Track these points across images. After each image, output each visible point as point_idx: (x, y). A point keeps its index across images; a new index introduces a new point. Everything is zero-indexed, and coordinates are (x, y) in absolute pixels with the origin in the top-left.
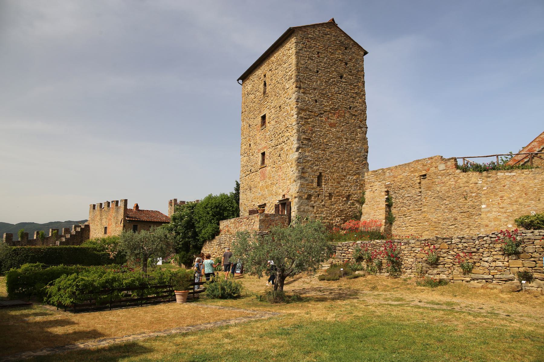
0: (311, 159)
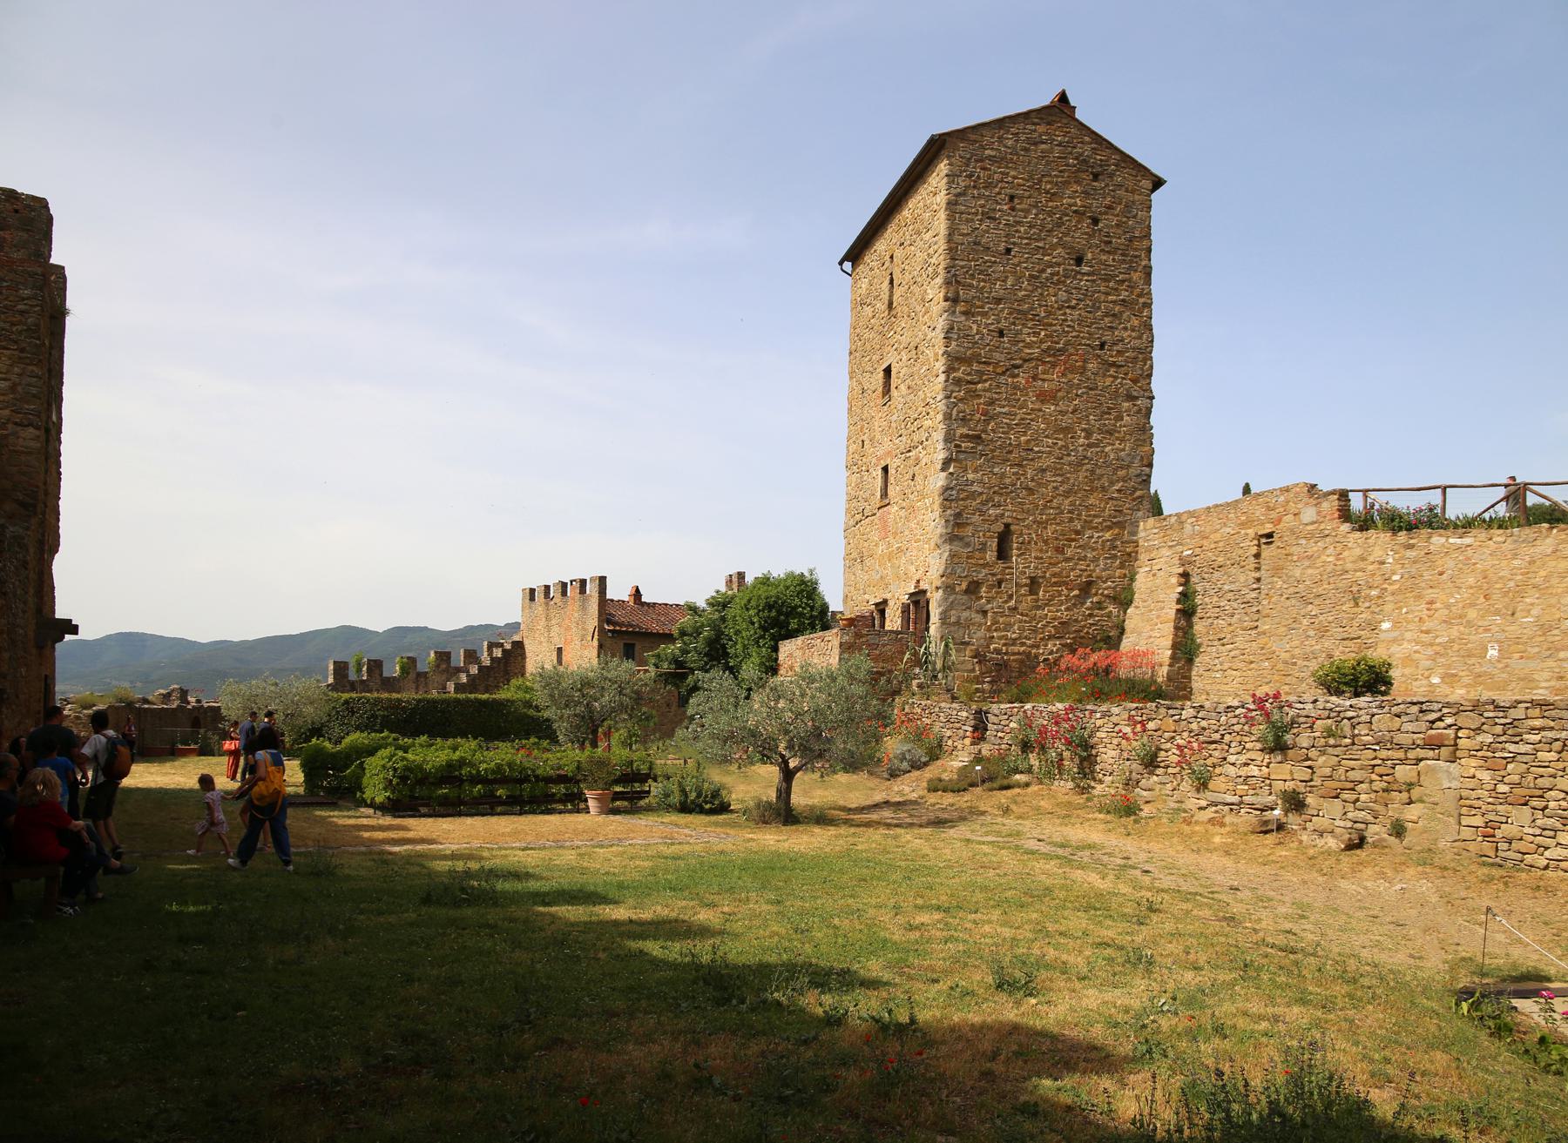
0: (980, 490)
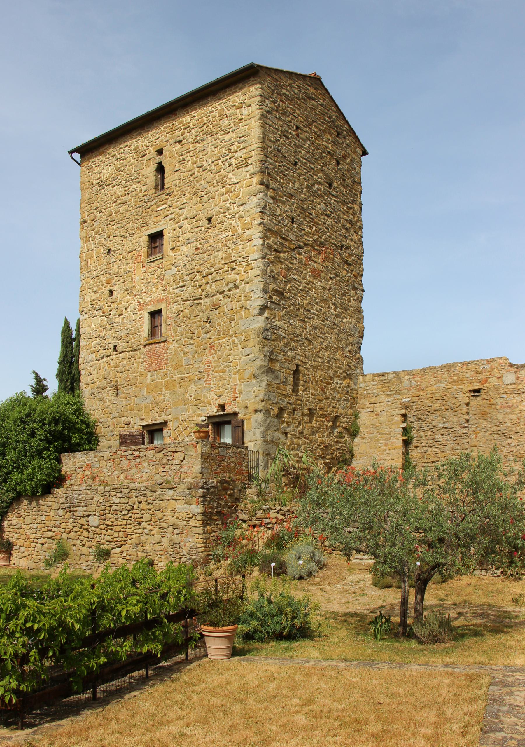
0: (283, 335)
